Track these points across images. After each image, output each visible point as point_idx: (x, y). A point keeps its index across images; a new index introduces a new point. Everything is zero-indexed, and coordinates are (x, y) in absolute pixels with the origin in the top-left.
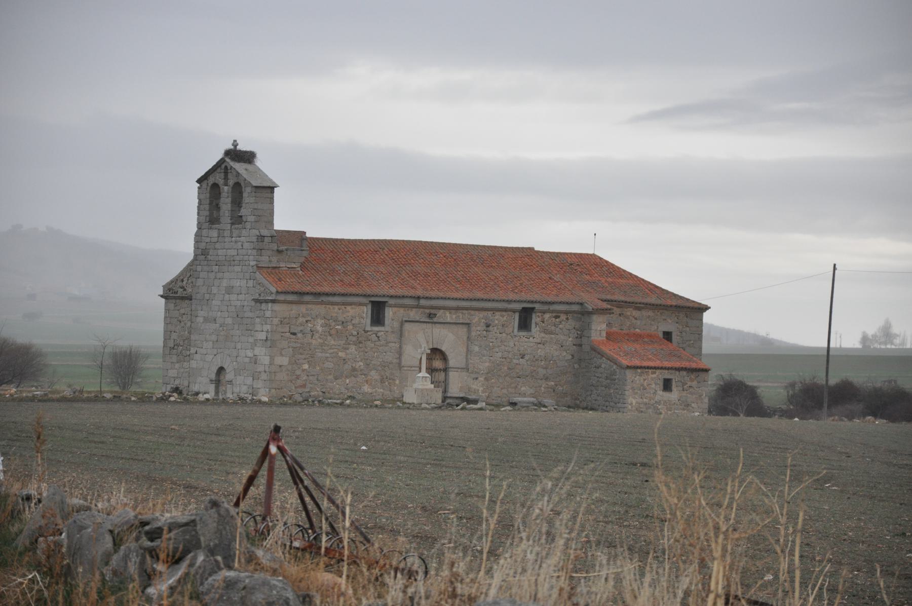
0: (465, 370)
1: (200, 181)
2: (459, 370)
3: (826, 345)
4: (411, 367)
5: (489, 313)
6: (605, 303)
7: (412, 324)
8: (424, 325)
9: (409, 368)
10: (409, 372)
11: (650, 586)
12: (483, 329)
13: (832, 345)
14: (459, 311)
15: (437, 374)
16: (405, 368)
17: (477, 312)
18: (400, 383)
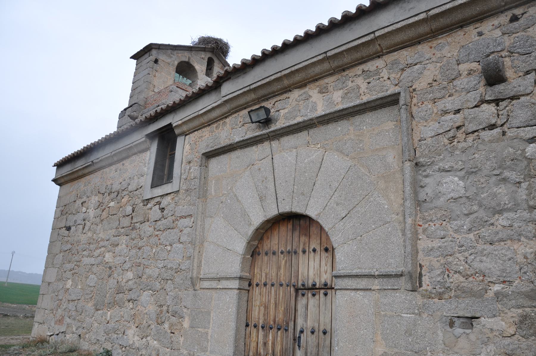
0: (403, 282)
1: (136, 57)
2: (376, 284)
3: (9, 269)
4: (219, 279)
5: (486, 26)
6: (255, 344)
7: (224, 158)
8: (255, 152)
9: (214, 284)
10: (214, 293)
11: (519, 99)
12: (474, 97)
13: (11, 270)
14: (351, 73)
15: (312, 302)
16: (206, 284)
17: (424, 49)
18: (192, 327)
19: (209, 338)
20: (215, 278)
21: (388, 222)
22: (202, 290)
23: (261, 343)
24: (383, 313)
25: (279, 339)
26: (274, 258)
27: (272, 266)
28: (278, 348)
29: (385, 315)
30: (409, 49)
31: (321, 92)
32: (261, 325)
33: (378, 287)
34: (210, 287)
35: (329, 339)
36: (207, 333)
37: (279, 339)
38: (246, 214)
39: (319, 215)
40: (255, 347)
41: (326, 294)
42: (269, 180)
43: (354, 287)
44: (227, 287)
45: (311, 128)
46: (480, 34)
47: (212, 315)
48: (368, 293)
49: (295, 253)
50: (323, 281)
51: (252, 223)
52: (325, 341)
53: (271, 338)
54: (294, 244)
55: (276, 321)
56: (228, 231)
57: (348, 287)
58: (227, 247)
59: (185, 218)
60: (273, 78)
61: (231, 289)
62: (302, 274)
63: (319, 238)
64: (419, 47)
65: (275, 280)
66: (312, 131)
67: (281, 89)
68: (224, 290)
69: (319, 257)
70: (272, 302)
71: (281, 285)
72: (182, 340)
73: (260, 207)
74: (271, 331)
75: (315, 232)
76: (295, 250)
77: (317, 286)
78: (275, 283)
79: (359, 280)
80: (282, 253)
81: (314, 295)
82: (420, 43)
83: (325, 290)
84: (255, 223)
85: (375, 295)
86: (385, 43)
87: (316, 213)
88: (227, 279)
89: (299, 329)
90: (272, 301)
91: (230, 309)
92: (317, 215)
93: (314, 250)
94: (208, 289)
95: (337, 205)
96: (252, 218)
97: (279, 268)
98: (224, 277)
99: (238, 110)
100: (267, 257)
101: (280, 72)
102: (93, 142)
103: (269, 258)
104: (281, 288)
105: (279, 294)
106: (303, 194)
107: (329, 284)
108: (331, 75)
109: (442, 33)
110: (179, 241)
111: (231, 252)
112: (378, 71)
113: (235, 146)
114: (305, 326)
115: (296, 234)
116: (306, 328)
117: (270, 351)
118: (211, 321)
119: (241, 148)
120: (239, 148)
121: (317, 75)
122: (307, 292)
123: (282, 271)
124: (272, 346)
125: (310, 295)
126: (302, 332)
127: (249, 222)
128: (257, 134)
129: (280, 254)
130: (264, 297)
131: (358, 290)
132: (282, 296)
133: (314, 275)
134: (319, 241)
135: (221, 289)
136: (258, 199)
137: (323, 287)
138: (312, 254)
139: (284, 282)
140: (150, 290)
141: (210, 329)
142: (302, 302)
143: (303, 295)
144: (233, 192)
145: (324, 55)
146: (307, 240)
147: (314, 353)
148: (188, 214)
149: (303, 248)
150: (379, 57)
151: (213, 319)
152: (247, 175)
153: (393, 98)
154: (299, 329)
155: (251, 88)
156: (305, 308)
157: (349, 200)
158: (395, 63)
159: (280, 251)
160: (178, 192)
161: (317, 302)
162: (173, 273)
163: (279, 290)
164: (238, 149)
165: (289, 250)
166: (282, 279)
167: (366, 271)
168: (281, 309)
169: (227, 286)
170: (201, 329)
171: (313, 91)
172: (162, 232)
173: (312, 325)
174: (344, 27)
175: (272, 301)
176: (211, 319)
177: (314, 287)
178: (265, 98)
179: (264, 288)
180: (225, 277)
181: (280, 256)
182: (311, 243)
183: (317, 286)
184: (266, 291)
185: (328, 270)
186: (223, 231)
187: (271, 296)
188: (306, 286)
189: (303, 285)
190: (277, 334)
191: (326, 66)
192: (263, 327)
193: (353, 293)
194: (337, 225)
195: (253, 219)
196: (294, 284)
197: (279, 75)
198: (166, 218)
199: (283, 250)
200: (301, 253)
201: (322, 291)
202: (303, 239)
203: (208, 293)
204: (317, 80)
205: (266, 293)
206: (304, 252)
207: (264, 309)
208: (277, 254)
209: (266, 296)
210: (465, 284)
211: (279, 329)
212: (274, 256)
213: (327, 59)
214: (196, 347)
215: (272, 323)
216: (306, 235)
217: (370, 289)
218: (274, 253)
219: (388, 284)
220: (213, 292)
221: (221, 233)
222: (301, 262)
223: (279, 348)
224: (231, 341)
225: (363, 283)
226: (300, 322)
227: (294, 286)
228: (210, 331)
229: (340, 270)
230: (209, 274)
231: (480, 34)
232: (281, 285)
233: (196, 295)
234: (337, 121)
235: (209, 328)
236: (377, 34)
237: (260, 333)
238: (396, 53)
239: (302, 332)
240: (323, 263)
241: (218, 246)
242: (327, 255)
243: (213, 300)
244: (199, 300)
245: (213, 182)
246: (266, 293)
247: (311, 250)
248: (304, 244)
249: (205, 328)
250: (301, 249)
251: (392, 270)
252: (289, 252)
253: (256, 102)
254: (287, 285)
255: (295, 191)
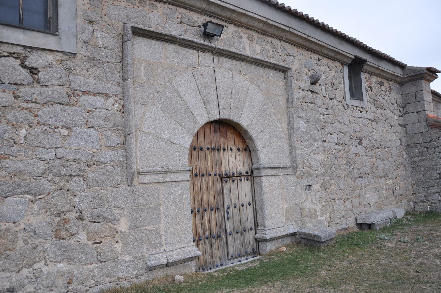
2: (280, 172)
4: (166, 173)
9: (160, 178)
16: (147, 178)
18: (133, 227)
19: (162, 232)
20: (163, 172)
21: (282, 138)
22: (142, 186)
23: (199, 224)
24: (284, 187)
25: (213, 217)
26: (202, 153)
27: (201, 159)
28: (213, 224)
29: (285, 189)
30: (291, 46)
31: (248, 38)
32: (197, 210)
33: (282, 174)
34: (154, 181)
35: (246, 209)
36: (158, 229)
37: (213, 217)
38: (190, 111)
39: (248, 126)
40: (194, 229)
41: (241, 180)
42: (211, 88)
43: (271, 174)
44: (177, 180)
45: (242, 61)
46: (311, 58)
47: (162, 209)
48: (277, 177)
49: (218, 150)
50: (239, 171)
51: (197, 121)
52: (243, 211)
53: (206, 218)
54: (217, 143)
55: (209, 204)
56: (170, 124)
57: (269, 175)
58: (172, 141)
59: (94, 95)
60: (232, 7)
61: (182, 181)
62: (225, 166)
63: (233, 141)
64: (294, 48)
65: (204, 171)
66: (243, 64)
67: (227, 18)
68: (174, 183)
69: (234, 154)
70: (204, 190)
71: (210, 175)
72: (119, 247)
73: (204, 109)
74: (206, 213)
75: (231, 136)
76: (218, 147)
77: (235, 175)
78: (205, 173)
79: (272, 170)
80: (208, 149)
81: (233, 181)
82: (295, 46)
83: (240, 177)
84: (200, 122)
85: (281, 178)
86: (289, 36)
87: (246, 124)
88: (177, 171)
89: (226, 206)
90: (204, 189)
91: (184, 200)
92: (247, 126)
93: (231, 149)
94: (152, 183)
95: (258, 122)
96: (197, 117)
97: (206, 162)
98: (175, 170)
99: (177, 4)
100: (195, 151)
101: (238, 7)
102: (435, 90)
103: (197, 153)
104: (210, 177)
105: (209, 182)
106: (237, 108)
107: (242, 173)
108: (257, 32)
109: (302, 48)
110: (87, 125)
111: (176, 145)
112: (277, 48)
113: (178, 40)
114: (230, 203)
115: (218, 135)
116: (231, 205)
117: (208, 229)
118: (162, 215)
119: (180, 45)
120: (178, 44)
121: (253, 27)
122: (229, 179)
123: (209, 164)
124: (208, 224)
125: (231, 181)
126: (228, 208)
127: (193, 119)
128: (195, 40)
129: (206, 150)
130: (197, 186)
131: (272, 176)
132: (212, 184)
133: (233, 167)
134: (233, 143)
135: (170, 182)
136: (201, 101)
137: (239, 175)
138: (230, 152)
139: (211, 173)
140: (26, 193)
141: (162, 223)
142: (226, 186)
143: (226, 182)
144: (173, 86)
145: (378, 67)
146: (225, 141)
147: (237, 221)
148: (100, 92)
149: (224, 147)
150: (280, 40)
151: (164, 213)
152: (189, 75)
153: (285, 69)
154: (226, 206)
155: (379, 72)
156: (229, 191)
157: (264, 121)
158: (285, 48)
159: (206, 148)
160: (74, 55)
161: (236, 186)
162: (83, 166)
163: (209, 179)
164: (176, 45)
165: (213, 147)
166: (210, 170)
167: (277, 165)
168: (212, 194)
169: (177, 178)
170: (150, 227)
171: (244, 35)
172: (39, 106)
173: (235, 202)
174: (277, 11)
175: (203, 188)
176: (162, 213)
177: (233, 175)
178: (210, 14)
179: (196, 178)
180: (176, 170)
181: (206, 152)
182: (228, 143)
183: (235, 175)
184: (197, 181)
185: (241, 163)
186: (163, 123)
187: (202, 185)
188: (228, 175)
189: (226, 175)
190: (211, 214)
191: (261, 26)
192: (198, 211)
193: (270, 178)
194: (259, 135)
195: (198, 118)
196: (220, 174)
197: (236, 9)
198: (46, 86)
199: (209, 147)
200: (222, 151)
201: (239, 178)
202: (223, 140)
203: (153, 188)
204: (249, 29)
205: (198, 182)
206: (224, 150)
207: (197, 196)
208: (204, 150)
209: (198, 185)
210: (309, 171)
211: (212, 210)
212: (202, 152)
213: (266, 23)
214: (145, 247)
215: (206, 206)
216: (224, 137)
217: (279, 175)
218: (201, 149)
219: (285, 171)
220: (160, 186)
221: (161, 125)
222: (222, 157)
223: (214, 224)
224: (189, 228)
225: (274, 172)
226: (226, 201)
227: (220, 175)
228: (162, 226)
229: (262, 164)
230: (149, 167)
231: (311, 58)
232: (210, 175)
233: (134, 192)
234: (257, 66)
235: (160, 223)
236: (291, 30)
237: (197, 217)
238: (286, 43)
239: (228, 208)
240: (238, 159)
241: (158, 137)
242: (239, 153)
243: (161, 194)
244: (140, 197)
245: (143, 65)
246: (198, 182)
247: (229, 149)
248: (224, 144)
249: (155, 224)
250: (222, 148)
251: (285, 164)
252: (214, 149)
253: (199, 11)
254: (214, 175)
255: (232, 104)
